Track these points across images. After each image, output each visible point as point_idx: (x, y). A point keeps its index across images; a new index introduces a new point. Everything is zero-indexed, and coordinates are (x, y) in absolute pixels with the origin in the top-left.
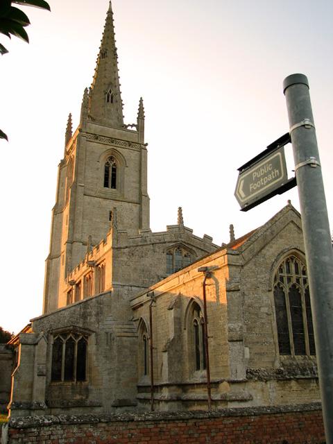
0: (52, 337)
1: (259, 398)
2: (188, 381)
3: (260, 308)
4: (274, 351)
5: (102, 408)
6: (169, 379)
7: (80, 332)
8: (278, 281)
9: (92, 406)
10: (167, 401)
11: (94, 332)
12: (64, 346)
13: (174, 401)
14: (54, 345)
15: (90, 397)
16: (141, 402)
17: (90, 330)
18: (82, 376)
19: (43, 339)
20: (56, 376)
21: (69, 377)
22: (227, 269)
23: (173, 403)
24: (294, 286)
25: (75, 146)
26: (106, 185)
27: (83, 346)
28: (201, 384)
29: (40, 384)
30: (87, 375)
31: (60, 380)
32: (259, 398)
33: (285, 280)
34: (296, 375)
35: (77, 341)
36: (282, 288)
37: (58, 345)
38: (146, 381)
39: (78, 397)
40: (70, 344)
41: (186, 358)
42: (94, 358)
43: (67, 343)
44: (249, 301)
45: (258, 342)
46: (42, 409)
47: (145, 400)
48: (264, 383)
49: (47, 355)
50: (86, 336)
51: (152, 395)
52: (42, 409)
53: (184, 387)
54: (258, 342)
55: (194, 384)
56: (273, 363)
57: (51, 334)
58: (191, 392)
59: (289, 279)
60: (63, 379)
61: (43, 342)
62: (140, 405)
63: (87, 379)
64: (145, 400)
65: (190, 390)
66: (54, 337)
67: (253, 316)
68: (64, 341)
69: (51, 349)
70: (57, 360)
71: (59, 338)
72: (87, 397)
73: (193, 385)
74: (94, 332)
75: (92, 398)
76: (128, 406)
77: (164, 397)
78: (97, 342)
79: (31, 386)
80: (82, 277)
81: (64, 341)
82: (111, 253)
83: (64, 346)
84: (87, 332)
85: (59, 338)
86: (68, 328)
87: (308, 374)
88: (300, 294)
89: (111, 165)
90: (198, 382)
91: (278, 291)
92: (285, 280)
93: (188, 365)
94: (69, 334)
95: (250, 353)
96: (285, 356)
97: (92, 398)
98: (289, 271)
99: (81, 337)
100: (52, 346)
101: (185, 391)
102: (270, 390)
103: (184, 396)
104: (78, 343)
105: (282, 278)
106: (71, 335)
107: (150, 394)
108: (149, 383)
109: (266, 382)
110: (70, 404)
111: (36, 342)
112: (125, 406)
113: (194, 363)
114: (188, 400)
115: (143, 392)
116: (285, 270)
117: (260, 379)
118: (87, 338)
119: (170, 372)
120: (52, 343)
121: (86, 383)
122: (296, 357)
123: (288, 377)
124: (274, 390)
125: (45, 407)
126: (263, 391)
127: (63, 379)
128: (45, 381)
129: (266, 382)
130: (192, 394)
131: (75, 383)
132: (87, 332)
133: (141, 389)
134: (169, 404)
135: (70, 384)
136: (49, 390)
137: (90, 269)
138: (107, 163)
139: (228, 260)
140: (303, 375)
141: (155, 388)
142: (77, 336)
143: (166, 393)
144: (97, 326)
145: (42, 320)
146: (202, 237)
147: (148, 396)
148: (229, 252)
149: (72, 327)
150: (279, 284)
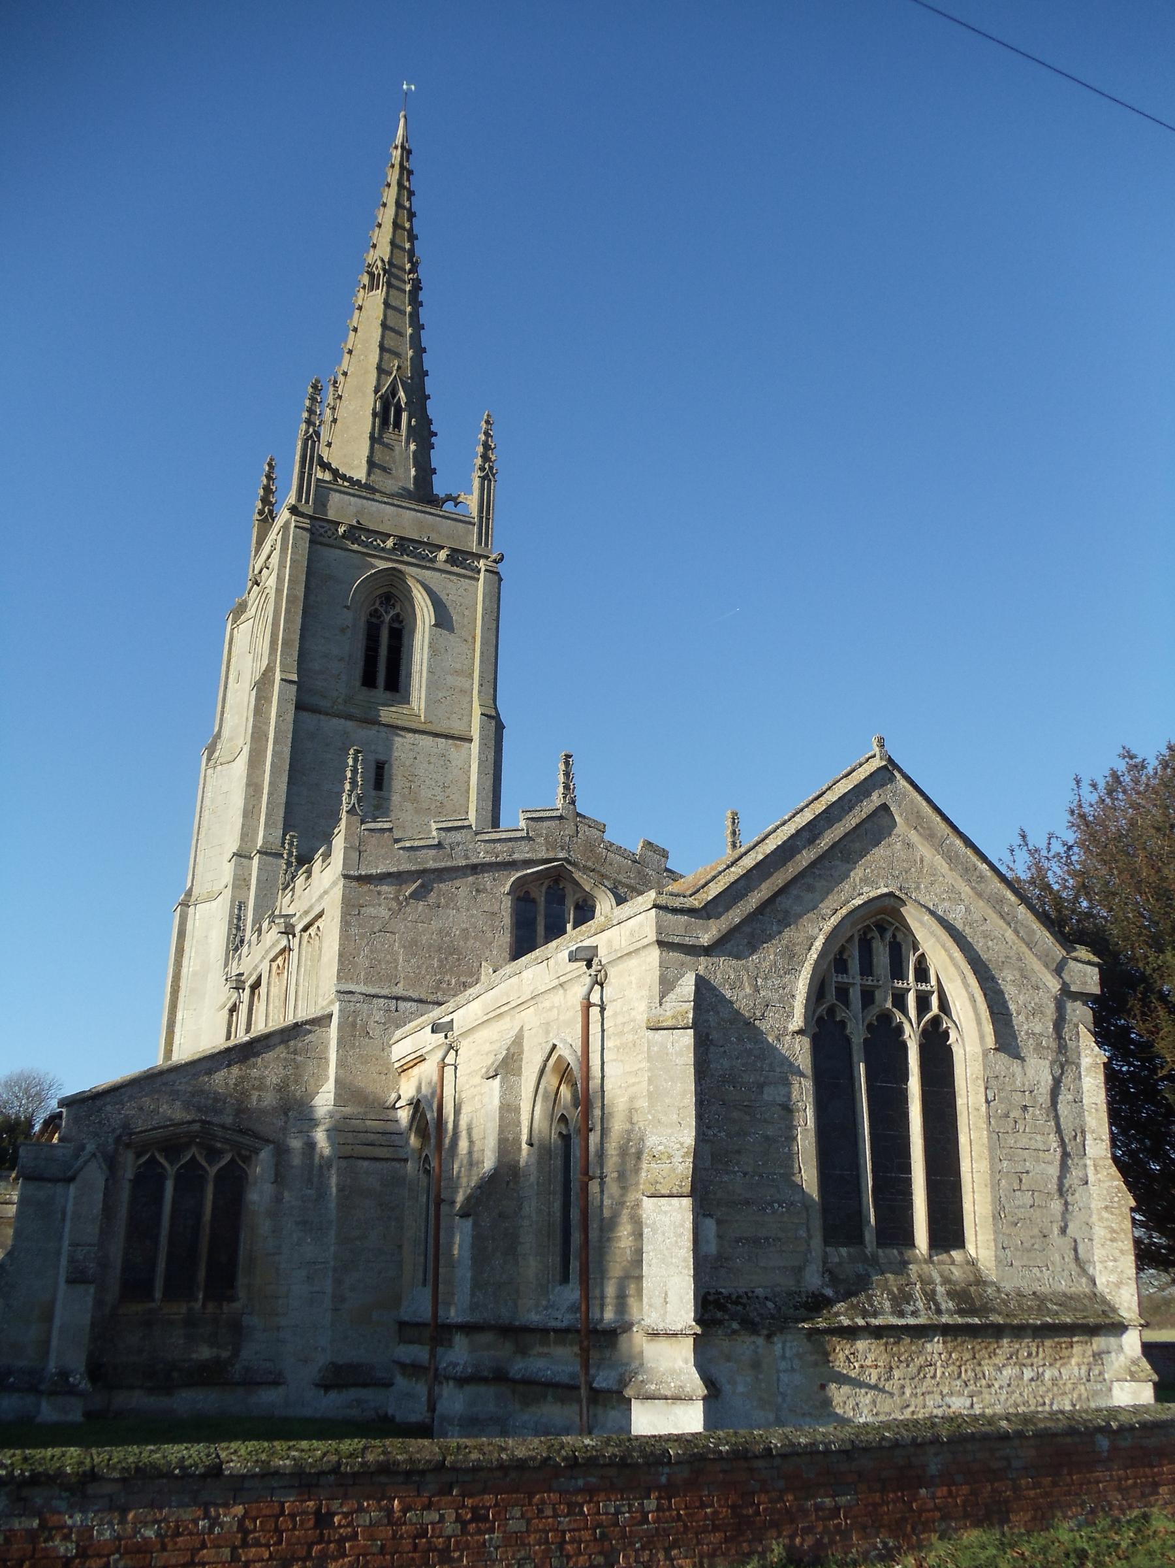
0: (130, 1156)
1: (741, 1389)
2: (535, 1318)
3: (761, 1086)
4: (802, 1233)
5: (281, 1390)
6: (474, 1307)
7: (226, 1141)
8: (831, 997)
9: (251, 1382)
10: (462, 1381)
11: (268, 1141)
12: (169, 1186)
13: (484, 1380)
14: (139, 1181)
15: (245, 1354)
16: (403, 1374)
17: (256, 1136)
18: (223, 1280)
19: (93, 1165)
20: (136, 1285)
21: (179, 1287)
22: (655, 953)
23: (482, 1389)
24: (936, 1021)
25: (275, 560)
26: (369, 680)
27: (233, 1184)
28: (567, 1331)
29: (74, 1311)
30: (241, 1280)
31: (153, 1300)
32: (741, 1389)
33: (855, 995)
34: (875, 1315)
35: (213, 1171)
36: (843, 1024)
37: (148, 1181)
38: (418, 1305)
39: (205, 1353)
40: (190, 1179)
41: (528, 1240)
42: (265, 1226)
43: (178, 1178)
44: (726, 1063)
45: (747, 1202)
46: (72, 1391)
47: (413, 1370)
48: (760, 1341)
49: (108, 1210)
50: (246, 1156)
51: (433, 1355)
52: (72, 1391)
53: (516, 1334)
54: (747, 1202)
55: (545, 1331)
56: (799, 1271)
57: (128, 1146)
58: (540, 1355)
59: (868, 997)
60: (158, 1295)
61: (95, 1175)
62: (401, 1382)
63: (242, 1294)
64: (413, 1370)
65: (539, 1349)
66: (138, 1155)
67: (735, 1115)
68: (171, 1170)
69: (125, 1195)
70: (141, 1228)
71: (152, 1161)
72: (236, 1353)
73: (543, 1332)
74: (268, 1141)
75: (251, 1353)
76: (365, 1385)
77: (455, 1365)
78: (276, 1175)
79: (48, 1317)
80: (266, 963)
81: (171, 1170)
82: (337, 893)
83: (169, 1186)
84: (246, 1140)
85: (152, 1161)
86: (184, 1128)
87: (915, 1314)
88: (848, 1041)
89: (387, 618)
90: (558, 1324)
91: (508, 1049)
92: (855, 995)
93: (532, 1265)
94: (188, 1146)
95: (719, 1237)
96: (844, 1251)
97: (251, 1353)
98: (867, 969)
99: (227, 1158)
100: (127, 1186)
101: (523, 1351)
102: (783, 1365)
103: (518, 1367)
104: (219, 1177)
105: (843, 993)
106: (194, 1150)
107: (427, 1348)
108: (426, 1314)
109: (769, 1337)
110: (175, 1375)
111: (70, 1174)
112: (355, 1385)
113: (555, 1260)
114: (528, 1382)
115: (411, 1342)
116: (854, 965)
117: (750, 1326)
118: (247, 1160)
119: (476, 1285)
120: (129, 1175)
121: (237, 1305)
122: (880, 1251)
123: (846, 1322)
124: (797, 1364)
125: (85, 1385)
126: (756, 1365)
127: (158, 1295)
128: (89, 1302)
129: (769, 1337)
130: (540, 1363)
131: (198, 1306)
132: (246, 1140)
133: (407, 1330)
134: (470, 1389)
135: (184, 1310)
136: (104, 1329)
137: (284, 943)
138: (375, 614)
139: (660, 930)
140: (901, 1314)
141: (440, 1333)
142: (213, 1154)
143: (460, 1354)
144: (281, 1123)
145: (98, 1103)
146: (638, 849)
147: (419, 1353)
148: (662, 901)
149: (196, 1127)
150: (831, 1011)
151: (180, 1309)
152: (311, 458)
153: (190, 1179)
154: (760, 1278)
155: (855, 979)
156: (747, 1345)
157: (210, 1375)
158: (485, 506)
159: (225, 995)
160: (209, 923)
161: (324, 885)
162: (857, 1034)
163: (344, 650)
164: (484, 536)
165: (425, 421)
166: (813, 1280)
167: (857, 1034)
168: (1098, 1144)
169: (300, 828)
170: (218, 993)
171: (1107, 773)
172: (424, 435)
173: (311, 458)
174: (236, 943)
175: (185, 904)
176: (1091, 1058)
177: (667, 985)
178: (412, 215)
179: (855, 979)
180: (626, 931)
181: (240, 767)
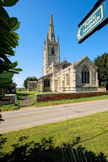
21: (47, 86)
33: (84, 70)
37: (45, 81)
39: (48, 89)
40: (47, 81)
59: (84, 70)
92: (84, 70)
98: (84, 69)
117: (78, 87)
151: (47, 87)
152: (48, 39)
153: (47, 81)
154: (79, 85)
155: (84, 69)
156: (78, 88)
157: (49, 90)
158: (58, 42)
159: (46, 72)
160: (45, 68)
161: (52, 65)
162: (84, 72)
163: (50, 52)
164: (58, 44)
165: (54, 36)
166: (81, 85)
167: (84, 72)
168: (97, 78)
169: (49, 64)
170: (45, 72)
171: (102, 55)
172: (54, 37)
173: (48, 39)
174: (46, 69)
175: (43, 67)
176: (97, 73)
177: (74, 70)
178: (53, 22)
179: (84, 69)
180: (71, 67)
181: (45, 59)
